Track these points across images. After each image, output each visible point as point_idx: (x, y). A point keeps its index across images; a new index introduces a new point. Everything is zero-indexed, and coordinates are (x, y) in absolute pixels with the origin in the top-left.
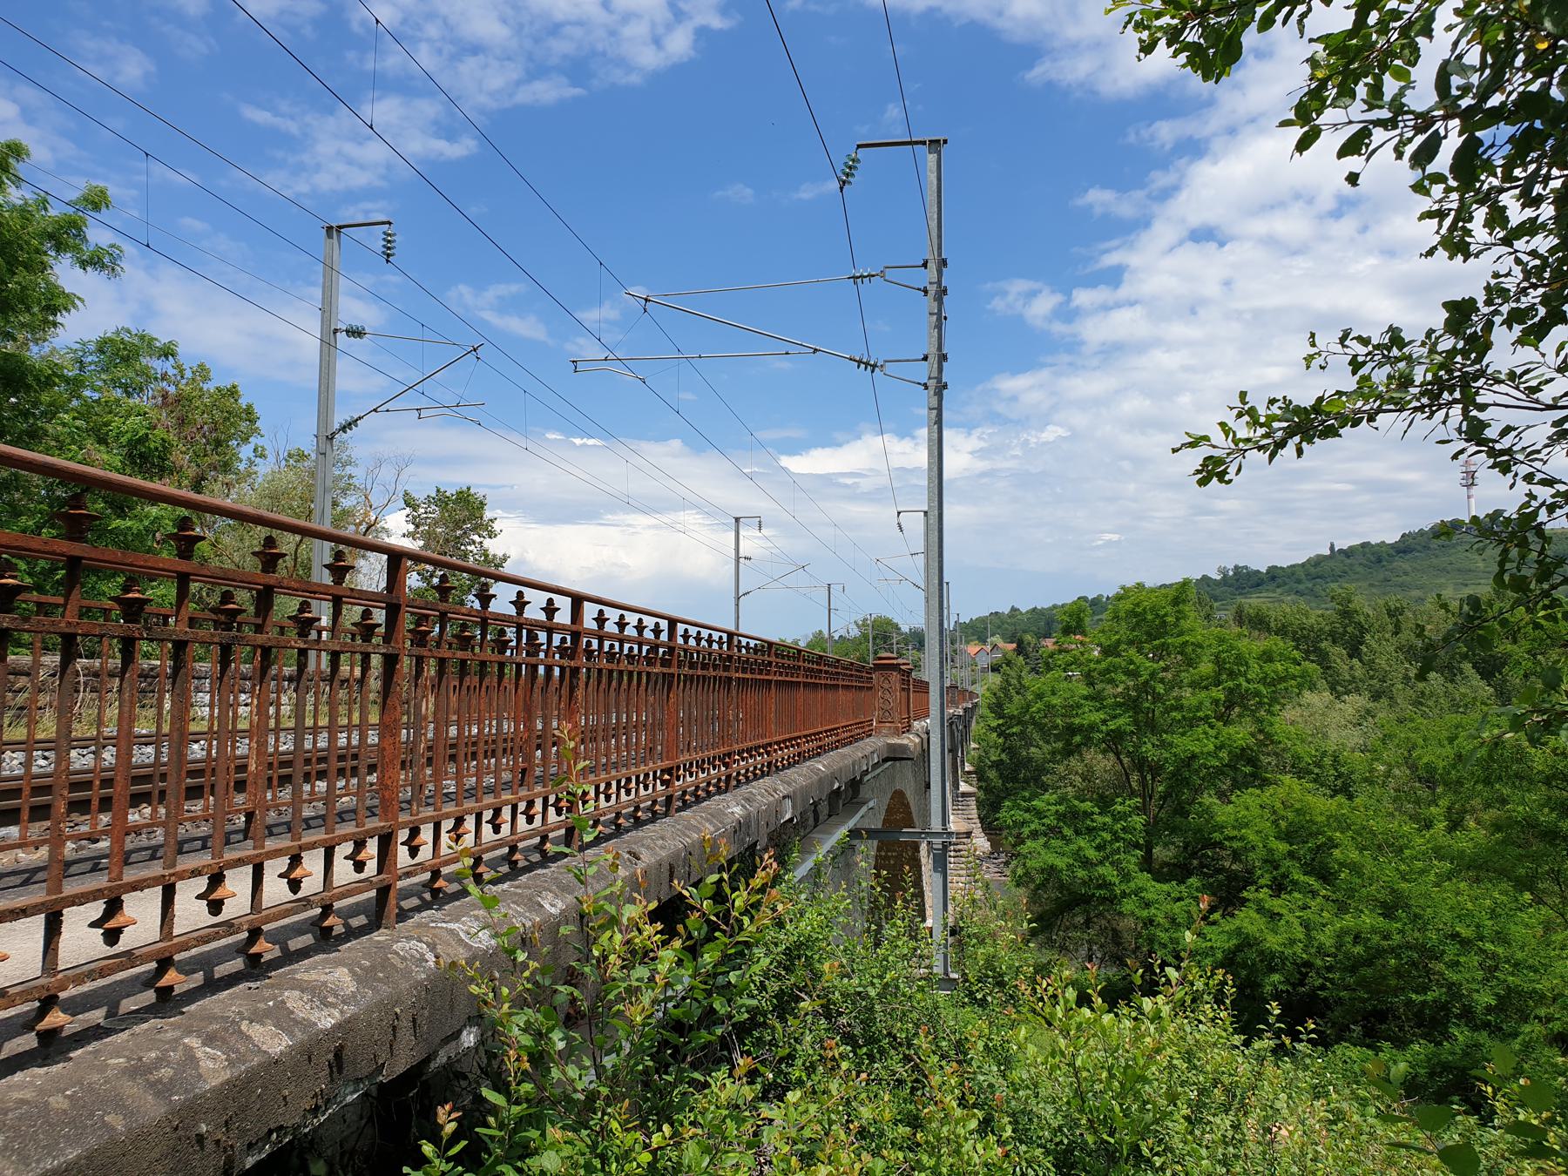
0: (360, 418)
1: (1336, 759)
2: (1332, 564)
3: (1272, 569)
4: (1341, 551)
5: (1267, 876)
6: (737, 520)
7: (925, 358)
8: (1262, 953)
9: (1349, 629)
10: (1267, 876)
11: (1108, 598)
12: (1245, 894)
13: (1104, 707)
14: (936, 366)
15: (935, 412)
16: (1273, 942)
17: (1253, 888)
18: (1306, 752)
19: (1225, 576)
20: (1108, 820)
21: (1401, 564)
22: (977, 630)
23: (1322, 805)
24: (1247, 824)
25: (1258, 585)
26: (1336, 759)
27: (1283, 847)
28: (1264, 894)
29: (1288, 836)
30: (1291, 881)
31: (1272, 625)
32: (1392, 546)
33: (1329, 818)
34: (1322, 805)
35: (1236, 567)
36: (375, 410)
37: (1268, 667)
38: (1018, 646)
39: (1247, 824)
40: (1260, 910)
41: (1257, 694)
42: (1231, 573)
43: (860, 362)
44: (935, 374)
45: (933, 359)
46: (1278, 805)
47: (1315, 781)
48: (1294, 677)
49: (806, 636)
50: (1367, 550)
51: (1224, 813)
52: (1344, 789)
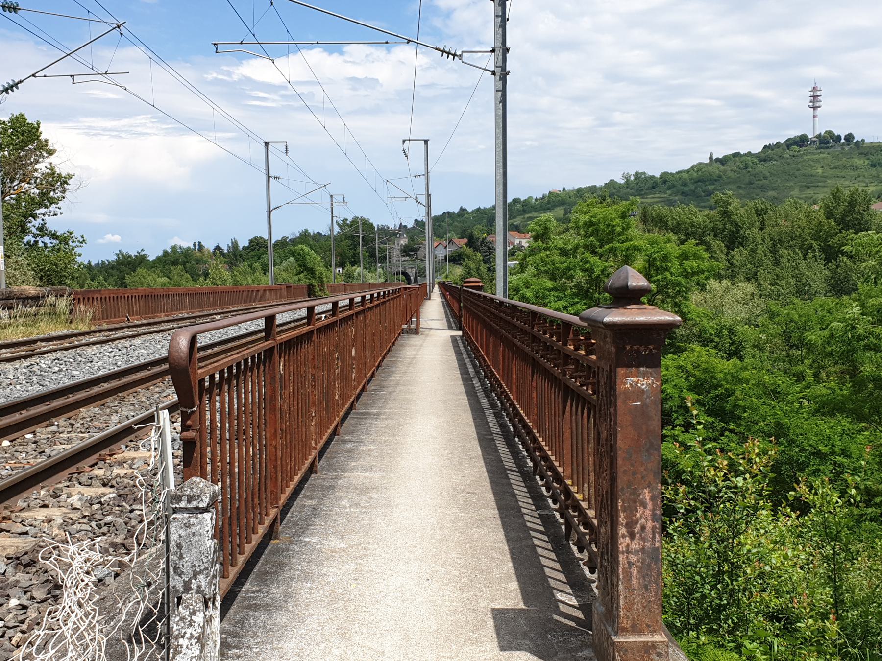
0: (21, 82)
1: (731, 331)
3: (664, 175)
4: (717, 160)
5: (680, 418)
6: (266, 144)
7: (493, 51)
9: (728, 226)
14: (500, 57)
15: (500, 93)
17: (670, 427)
18: (710, 326)
23: (724, 366)
24: (667, 381)
25: (653, 188)
26: (731, 331)
28: (678, 431)
29: (696, 388)
31: (670, 223)
33: (726, 374)
34: (724, 366)
36: (34, 75)
37: (687, 264)
38: (469, 241)
39: (667, 381)
41: (678, 284)
42: (632, 178)
43: (443, 52)
44: (500, 63)
45: (499, 52)
46: (690, 367)
47: (716, 347)
48: (703, 272)
50: (737, 159)
52: (735, 352)
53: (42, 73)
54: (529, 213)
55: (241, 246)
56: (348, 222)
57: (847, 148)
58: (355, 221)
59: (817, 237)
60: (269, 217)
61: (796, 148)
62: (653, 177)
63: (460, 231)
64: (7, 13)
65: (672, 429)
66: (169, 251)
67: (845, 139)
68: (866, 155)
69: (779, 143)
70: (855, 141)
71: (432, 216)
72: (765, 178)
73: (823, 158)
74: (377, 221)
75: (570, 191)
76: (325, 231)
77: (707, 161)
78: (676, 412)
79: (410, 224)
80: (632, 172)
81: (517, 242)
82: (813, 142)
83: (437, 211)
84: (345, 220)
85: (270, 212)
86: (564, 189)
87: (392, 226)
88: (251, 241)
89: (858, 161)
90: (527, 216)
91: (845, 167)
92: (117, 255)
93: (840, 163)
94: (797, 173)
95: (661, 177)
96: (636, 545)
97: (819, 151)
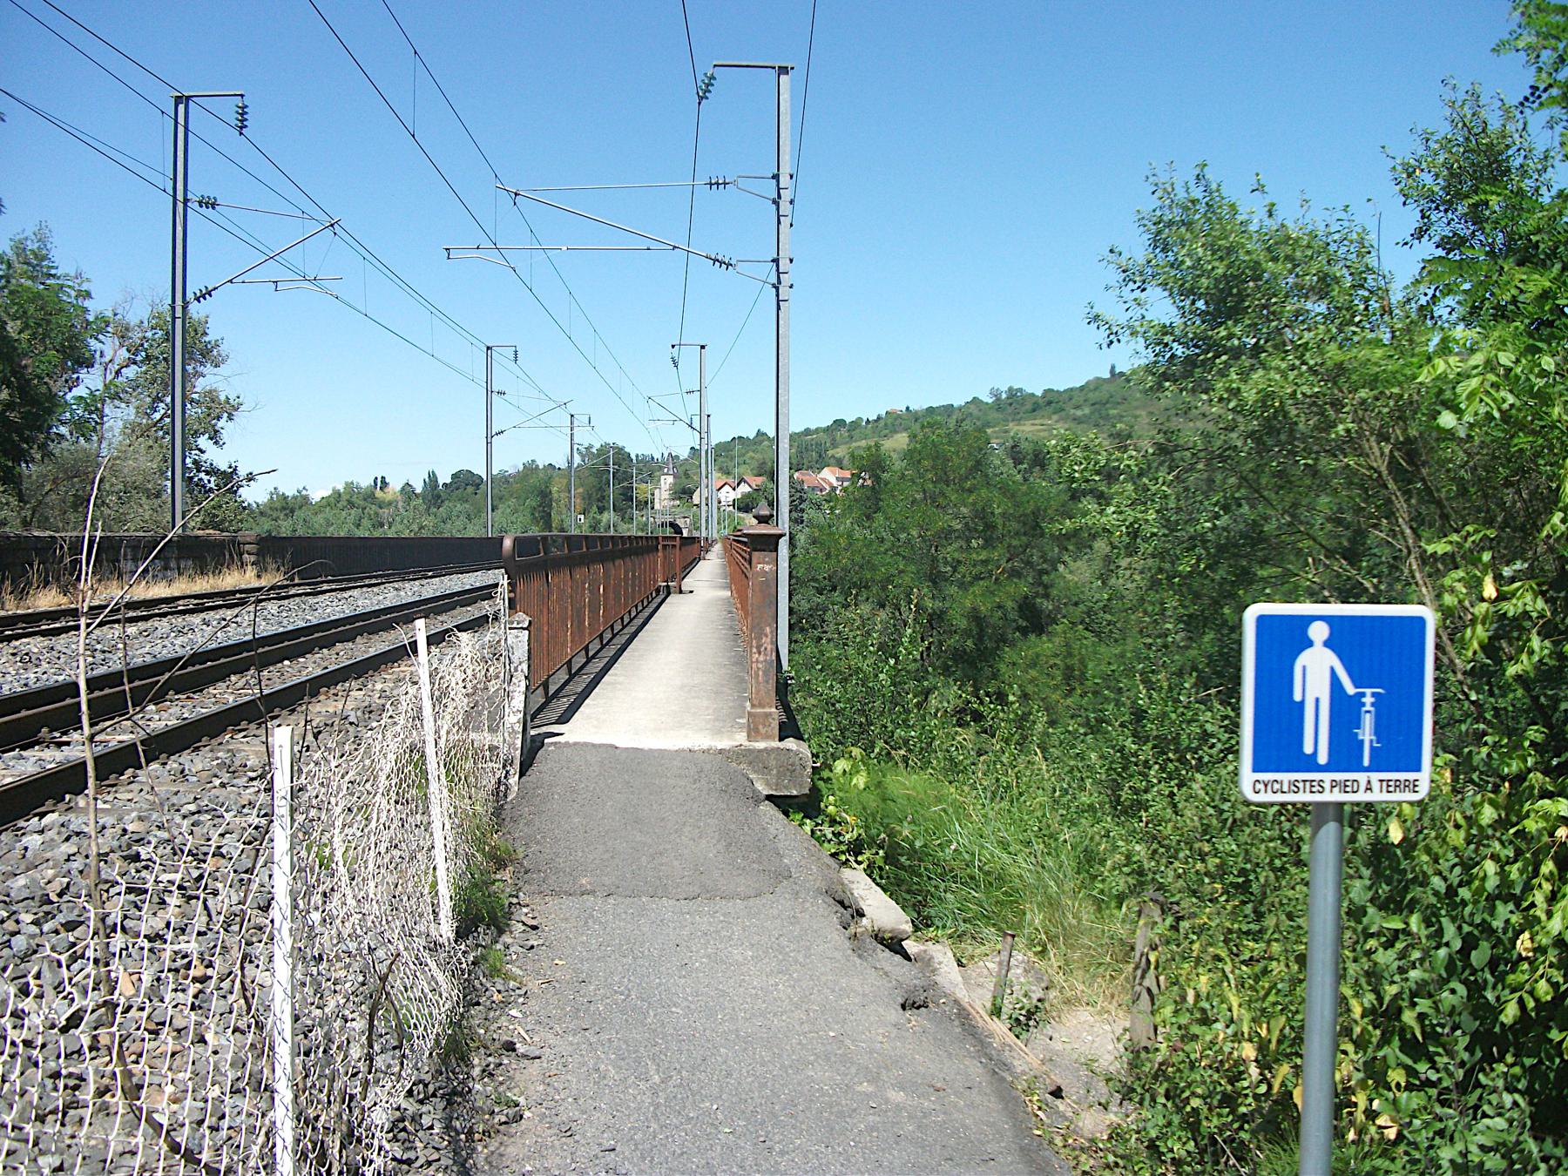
0: (215, 289)
2: (1112, 388)
19: (998, 398)
25: (1034, 410)
35: (1010, 389)
42: (1004, 396)
51: (1387, 988)
53: (240, 279)
55: (441, 482)
56: (594, 450)
58: (604, 449)
62: (1033, 395)
64: (204, 210)
71: (713, 443)
74: (634, 450)
75: (916, 412)
76: (561, 463)
77: (1107, 376)
79: (684, 453)
80: (1004, 388)
83: (720, 435)
84: (591, 446)
86: (908, 408)
87: (657, 456)
88: (454, 476)
95: (1043, 397)
96: (762, 658)
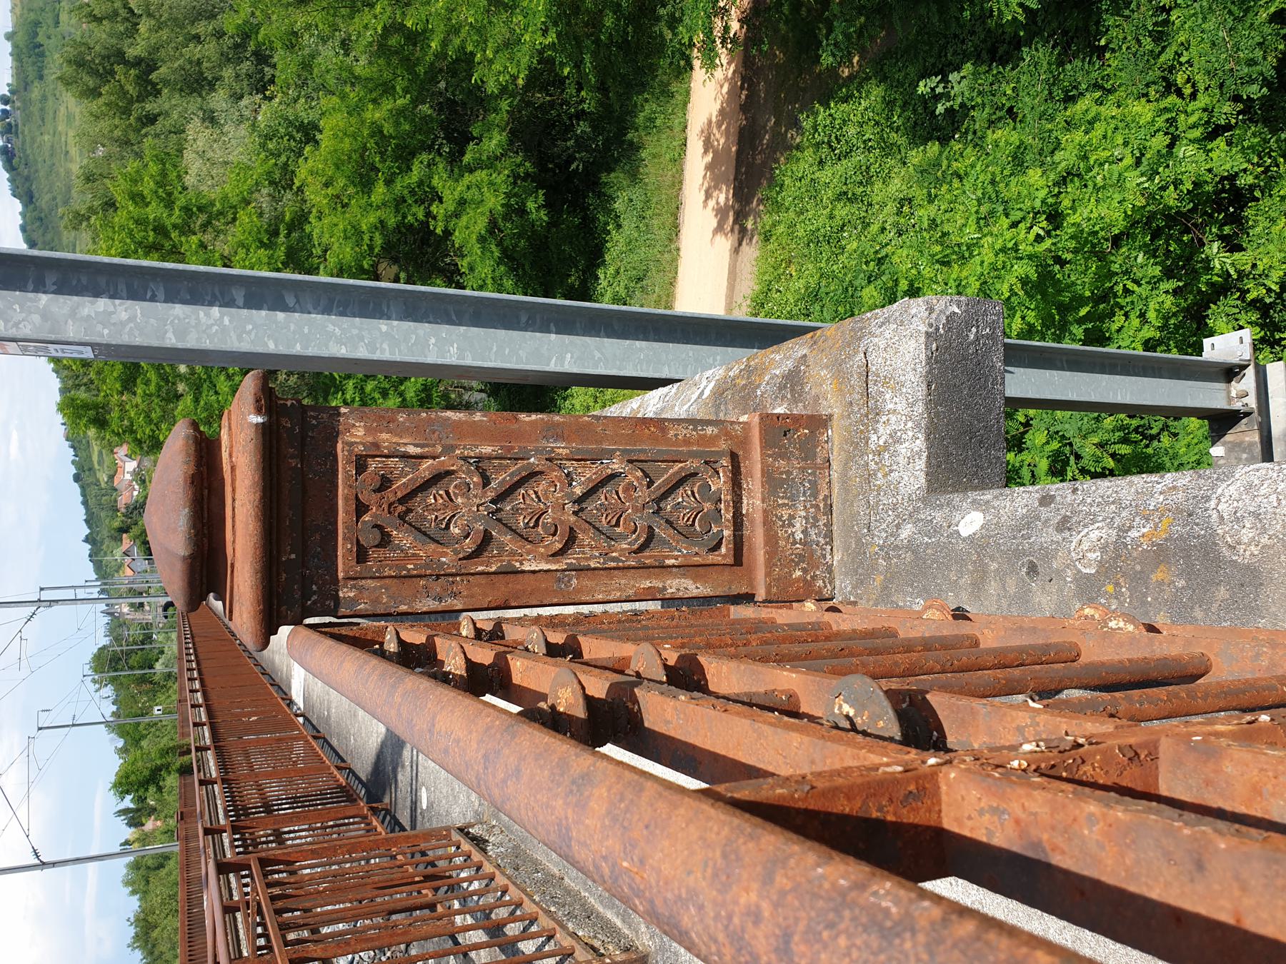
8: (506, 217)
10: (414, 209)
11: (75, 456)
12: (439, 231)
13: (209, 377)
16: (494, 202)
17: (432, 223)
20: (350, 384)
21: (43, 201)
22: (103, 571)
27: (380, 191)
29: (366, 185)
30: (419, 187)
32: (25, 205)
40: (457, 215)
49: (112, 740)
50: (28, 228)
54: (93, 465)
57: (18, 104)
59: (126, 112)
60: (54, 864)
61: (15, 161)
63: (113, 543)
65: (434, 218)
66: (130, 889)
67: (6, 105)
68: (27, 84)
69: (8, 180)
70: (8, 94)
72: (54, 199)
73: (30, 131)
78: (404, 217)
81: (128, 477)
82: (8, 141)
85: (44, 864)
89: (35, 93)
90: (96, 466)
91: (42, 109)
92: (135, 948)
93: (37, 113)
94: (48, 163)
97: (20, 136)
